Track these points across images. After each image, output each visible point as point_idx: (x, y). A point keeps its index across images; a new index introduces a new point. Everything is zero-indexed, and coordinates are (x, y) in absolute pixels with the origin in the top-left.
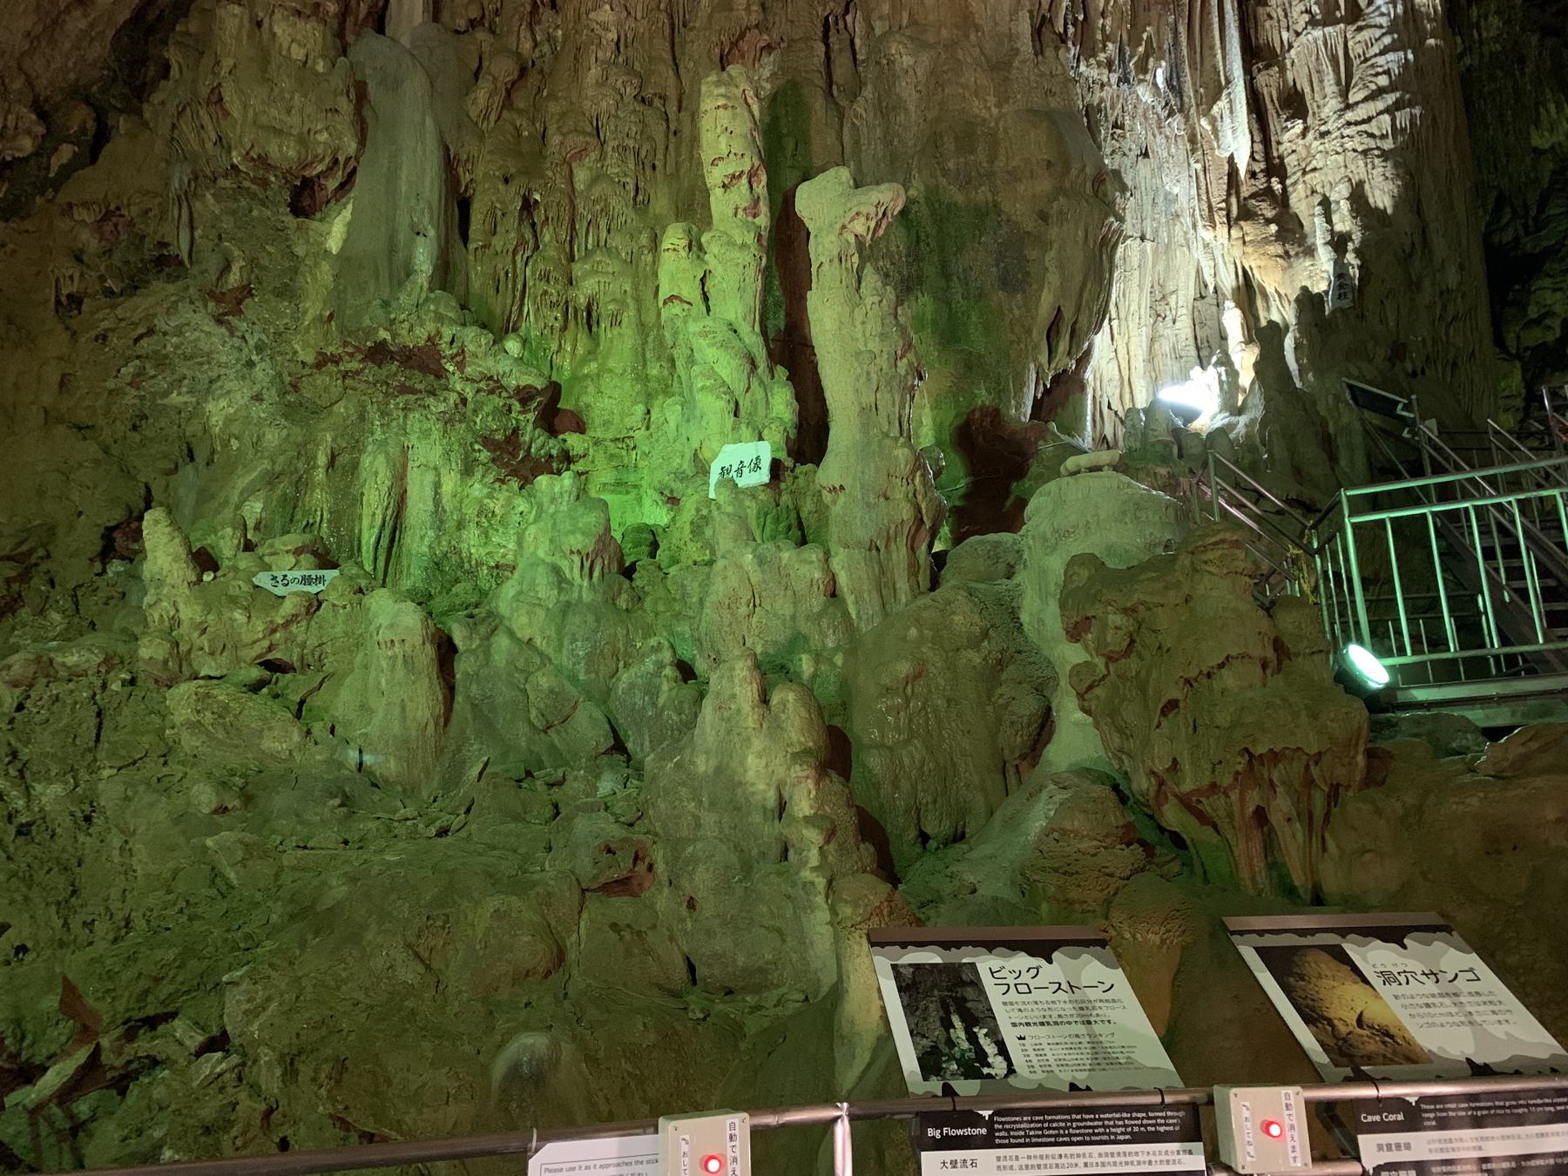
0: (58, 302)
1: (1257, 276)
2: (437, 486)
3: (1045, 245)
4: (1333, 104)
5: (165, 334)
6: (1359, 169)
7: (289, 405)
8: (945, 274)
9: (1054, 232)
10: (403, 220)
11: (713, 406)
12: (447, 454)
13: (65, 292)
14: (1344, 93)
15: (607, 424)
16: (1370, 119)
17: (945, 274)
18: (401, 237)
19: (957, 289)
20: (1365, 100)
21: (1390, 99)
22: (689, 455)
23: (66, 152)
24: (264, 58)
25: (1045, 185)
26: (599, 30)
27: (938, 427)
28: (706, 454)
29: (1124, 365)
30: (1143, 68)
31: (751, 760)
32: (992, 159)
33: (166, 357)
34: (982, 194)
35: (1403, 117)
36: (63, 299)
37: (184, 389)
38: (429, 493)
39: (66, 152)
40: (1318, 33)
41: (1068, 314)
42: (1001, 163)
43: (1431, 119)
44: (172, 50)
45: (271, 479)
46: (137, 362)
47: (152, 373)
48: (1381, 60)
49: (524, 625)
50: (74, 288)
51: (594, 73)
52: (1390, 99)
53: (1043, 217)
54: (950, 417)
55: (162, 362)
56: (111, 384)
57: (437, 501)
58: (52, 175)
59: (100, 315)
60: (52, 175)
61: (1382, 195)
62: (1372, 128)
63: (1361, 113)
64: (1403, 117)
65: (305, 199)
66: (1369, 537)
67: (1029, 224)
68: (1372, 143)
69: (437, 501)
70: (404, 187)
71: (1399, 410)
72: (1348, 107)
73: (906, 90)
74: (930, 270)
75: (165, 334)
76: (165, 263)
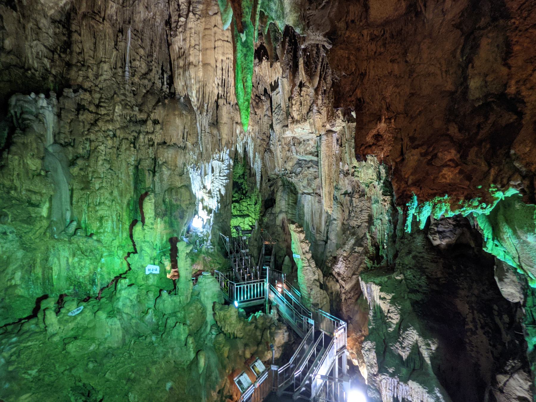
1: (204, 198)
2: (67, 260)
3: (187, 212)
4: (218, 174)
6: (220, 187)
8: (171, 214)
9: (188, 210)
10: (64, 208)
11: (147, 259)
12: (70, 254)
14: (220, 173)
15: (106, 243)
17: (171, 214)
18: (64, 212)
19: (173, 218)
21: (226, 178)
25: (188, 202)
26: (101, 152)
27: (167, 238)
30: (197, 170)
31: (182, 337)
32: (181, 197)
34: (179, 203)
35: (227, 181)
38: (65, 262)
40: (218, 162)
42: (182, 199)
43: (230, 182)
45: (22, 267)
49: (127, 310)
51: (100, 163)
52: (226, 178)
53: (187, 208)
54: (169, 237)
57: (68, 263)
61: (223, 192)
64: (227, 181)
66: (237, 288)
67: (185, 209)
69: (68, 263)
70: (63, 200)
72: (220, 176)
73: (165, 177)
74: (168, 213)
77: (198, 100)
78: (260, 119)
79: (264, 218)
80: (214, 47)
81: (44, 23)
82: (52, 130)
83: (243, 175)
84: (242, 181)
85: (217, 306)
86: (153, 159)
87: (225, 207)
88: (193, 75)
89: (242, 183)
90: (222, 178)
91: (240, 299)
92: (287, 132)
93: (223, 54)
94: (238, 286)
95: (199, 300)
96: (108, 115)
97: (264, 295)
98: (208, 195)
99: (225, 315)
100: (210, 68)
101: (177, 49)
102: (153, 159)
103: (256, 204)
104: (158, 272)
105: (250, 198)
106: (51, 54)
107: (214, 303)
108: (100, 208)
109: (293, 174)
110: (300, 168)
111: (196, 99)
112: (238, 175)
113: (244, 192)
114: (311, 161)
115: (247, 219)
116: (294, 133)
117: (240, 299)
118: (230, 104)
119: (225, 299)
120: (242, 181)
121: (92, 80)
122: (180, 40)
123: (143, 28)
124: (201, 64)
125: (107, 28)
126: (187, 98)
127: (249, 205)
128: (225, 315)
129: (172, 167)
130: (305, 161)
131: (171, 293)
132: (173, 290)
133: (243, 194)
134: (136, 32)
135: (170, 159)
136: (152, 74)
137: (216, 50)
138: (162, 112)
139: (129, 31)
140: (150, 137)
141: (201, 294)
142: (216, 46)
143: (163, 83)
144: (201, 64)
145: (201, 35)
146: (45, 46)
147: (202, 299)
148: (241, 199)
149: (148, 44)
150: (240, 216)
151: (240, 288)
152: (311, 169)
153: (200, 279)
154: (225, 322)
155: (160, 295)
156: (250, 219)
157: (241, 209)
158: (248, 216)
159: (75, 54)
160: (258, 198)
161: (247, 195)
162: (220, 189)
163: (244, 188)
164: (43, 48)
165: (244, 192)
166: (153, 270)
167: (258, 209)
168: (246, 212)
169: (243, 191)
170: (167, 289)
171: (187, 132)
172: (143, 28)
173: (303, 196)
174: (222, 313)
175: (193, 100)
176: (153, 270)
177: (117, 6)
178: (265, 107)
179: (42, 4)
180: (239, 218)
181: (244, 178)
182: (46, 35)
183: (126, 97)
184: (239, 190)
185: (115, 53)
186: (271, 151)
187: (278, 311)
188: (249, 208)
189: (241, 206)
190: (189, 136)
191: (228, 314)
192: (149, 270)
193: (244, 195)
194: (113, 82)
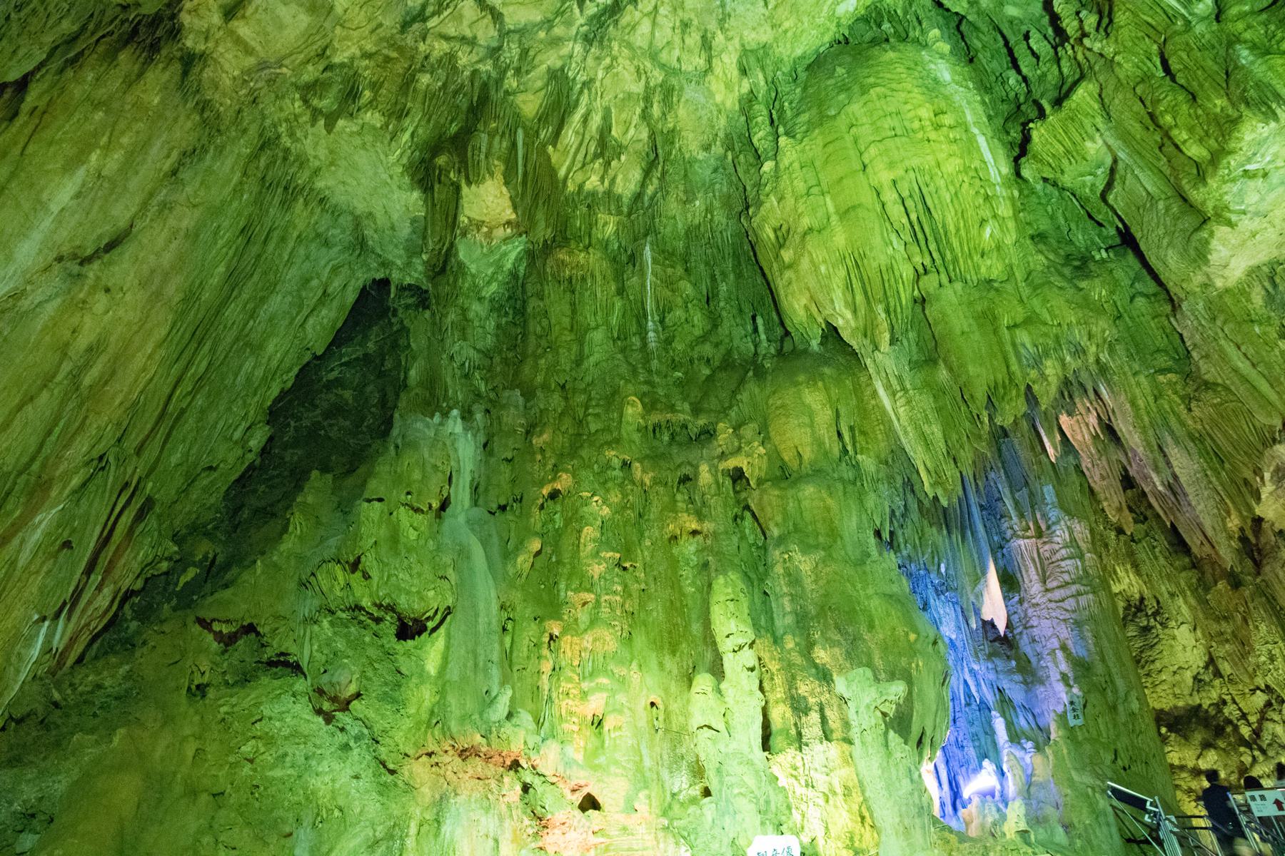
0: (189, 689)
5: (270, 719)
7: (385, 785)
13: (196, 682)
16: (1063, 600)
20: (1058, 587)
21: (1074, 588)
22: (726, 841)
23: (191, 573)
24: (394, 538)
28: (741, 842)
29: (186, 355)
33: (272, 737)
36: (193, 687)
37: (288, 765)
39: (191, 573)
41: (929, 733)
44: (297, 514)
46: (253, 742)
47: (262, 750)
48: (1063, 564)
50: (205, 680)
55: (269, 740)
56: (231, 759)
58: (178, 589)
59: (221, 702)
60: (178, 589)
62: (1066, 605)
63: (1058, 594)
65: (410, 629)
68: (1068, 616)
71: (1148, 806)
72: (1047, 590)
75: (270, 719)
76: (286, 665)
77: (855, 312)
80: (860, 167)
81: (477, 309)
82: (468, 478)
83: (1211, 661)
88: (819, 255)
90: (1058, 594)
93: (891, 165)
96: (607, 429)
98: (1018, 677)
100: (861, 213)
101: (772, 236)
106: (487, 362)
108: (593, 684)
111: (849, 315)
112: (1188, 676)
113: (1245, 731)
121: (568, 369)
123: (688, 247)
124: (834, 218)
125: (593, 260)
126: (831, 333)
129: (821, 539)
134: (665, 255)
136: (723, 330)
137: (869, 170)
138: (757, 390)
139: (648, 248)
142: (866, 162)
144: (834, 218)
145: (817, 164)
146: (479, 351)
149: (704, 273)
159: (532, 339)
164: (472, 353)
171: (852, 429)
172: (688, 247)
177: (617, 219)
179: (473, 276)
181: (1218, 674)
182: (480, 330)
183: (654, 387)
184: (1219, 732)
185: (618, 304)
190: (859, 438)
194: (616, 362)
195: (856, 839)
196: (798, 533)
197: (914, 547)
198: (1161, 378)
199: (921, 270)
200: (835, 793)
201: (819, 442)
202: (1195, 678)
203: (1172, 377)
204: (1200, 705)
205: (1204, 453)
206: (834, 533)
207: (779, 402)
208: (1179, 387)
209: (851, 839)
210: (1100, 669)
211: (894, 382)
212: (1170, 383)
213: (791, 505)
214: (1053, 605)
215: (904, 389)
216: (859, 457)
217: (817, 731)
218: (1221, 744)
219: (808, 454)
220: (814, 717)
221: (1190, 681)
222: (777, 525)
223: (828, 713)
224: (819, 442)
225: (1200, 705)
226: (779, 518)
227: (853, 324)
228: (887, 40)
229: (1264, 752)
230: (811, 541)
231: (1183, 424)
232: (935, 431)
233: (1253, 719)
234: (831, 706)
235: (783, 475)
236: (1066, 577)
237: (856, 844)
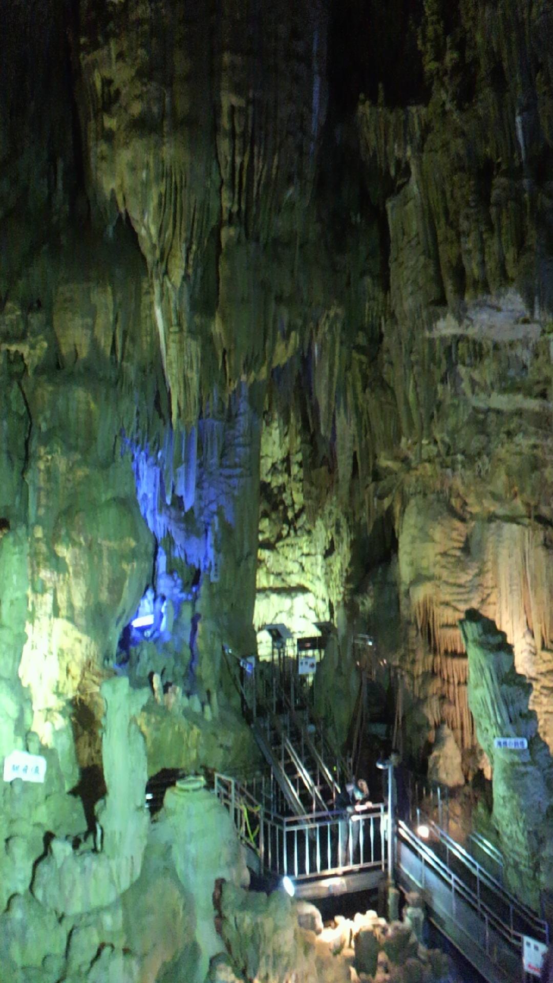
78: (348, 284)
79: (359, 599)
83: (287, 460)
84: (281, 479)
85: (230, 895)
86: (21, 418)
87: (238, 564)
89: (282, 488)
91: (302, 871)
92: (441, 324)
94: (372, 863)
95: (169, 870)
97: (378, 857)
99: (256, 926)
101: (99, 85)
102: (21, 418)
103: (328, 553)
104: (40, 778)
105: (309, 532)
107: (220, 884)
109: (459, 457)
110: (482, 438)
111: (153, 230)
113: (290, 515)
114: (519, 413)
115: (300, 599)
116: (466, 322)
117: (302, 871)
118: (257, 240)
119: (250, 869)
120: (281, 479)
122: (109, 55)
127: (308, 555)
128: (256, 926)
130: (498, 412)
131: (82, 847)
132: (86, 835)
133: (285, 520)
135: (72, 415)
140: (13, 348)
141: (177, 854)
143: (52, 188)
147: (180, 867)
148: (280, 538)
150: (278, 591)
151: (367, 859)
152: (519, 438)
153: (171, 797)
154: (257, 948)
155: (47, 852)
156: (309, 597)
157: (281, 569)
158: (303, 589)
160: (338, 532)
161: (300, 523)
162: (220, 508)
163: (288, 502)
165: (290, 515)
166: (25, 770)
167: (336, 568)
168: (294, 580)
169: (286, 510)
170: (64, 831)
173: (493, 525)
174: (247, 919)
175: (143, 232)
176: (25, 770)
178: (362, 248)
180: (274, 597)
181: (288, 470)
184: (275, 508)
186: (385, 386)
187: (428, 910)
188: (307, 566)
189: (281, 559)
191: (269, 924)
192: (15, 768)
193: (291, 523)
195: (61, 686)
196: (60, 432)
197: (144, 434)
198: (355, 355)
199: (226, 216)
200: (51, 653)
201: (94, 343)
202: (273, 465)
203: (364, 358)
204: (269, 484)
205: (359, 423)
206: (91, 437)
207: (68, 295)
208: (364, 367)
209: (58, 687)
210: (238, 535)
211: (173, 316)
212: (361, 363)
213: (61, 402)
214: (222, 479)
215: (179, 324)
216: (125, 364)
217: (49, 608)
218: (274, 516)
219: (84, 353)
220: (48, 598)
221: (269, 465)
222: (45, 420)
223: (59, 595)
224: (94, 343)
225: (269, 484)
226: (48, 414)
227: (155, 240)
228: (446, 652)
229: (296, 531)
230: (72, 441)
231: (355, 397)
232: (194, 377)
233: (297, 507)
234: (62, 591)
235: (55, 367)
236: (237, 460)
237: (60, 689)
